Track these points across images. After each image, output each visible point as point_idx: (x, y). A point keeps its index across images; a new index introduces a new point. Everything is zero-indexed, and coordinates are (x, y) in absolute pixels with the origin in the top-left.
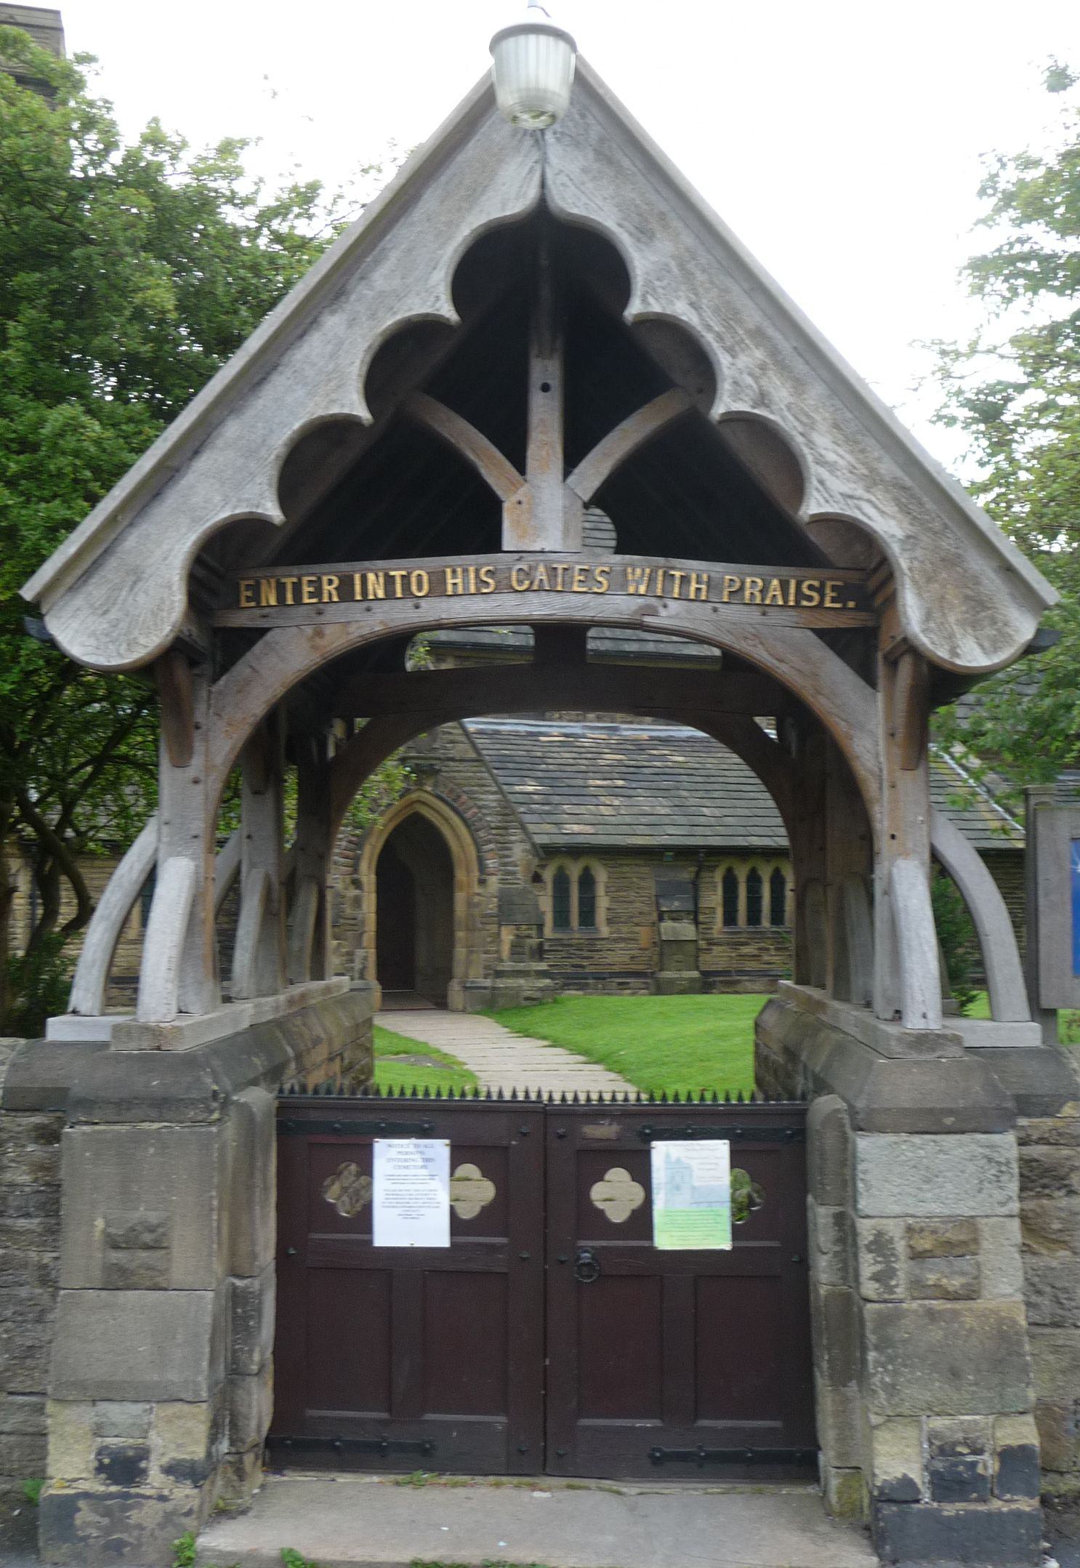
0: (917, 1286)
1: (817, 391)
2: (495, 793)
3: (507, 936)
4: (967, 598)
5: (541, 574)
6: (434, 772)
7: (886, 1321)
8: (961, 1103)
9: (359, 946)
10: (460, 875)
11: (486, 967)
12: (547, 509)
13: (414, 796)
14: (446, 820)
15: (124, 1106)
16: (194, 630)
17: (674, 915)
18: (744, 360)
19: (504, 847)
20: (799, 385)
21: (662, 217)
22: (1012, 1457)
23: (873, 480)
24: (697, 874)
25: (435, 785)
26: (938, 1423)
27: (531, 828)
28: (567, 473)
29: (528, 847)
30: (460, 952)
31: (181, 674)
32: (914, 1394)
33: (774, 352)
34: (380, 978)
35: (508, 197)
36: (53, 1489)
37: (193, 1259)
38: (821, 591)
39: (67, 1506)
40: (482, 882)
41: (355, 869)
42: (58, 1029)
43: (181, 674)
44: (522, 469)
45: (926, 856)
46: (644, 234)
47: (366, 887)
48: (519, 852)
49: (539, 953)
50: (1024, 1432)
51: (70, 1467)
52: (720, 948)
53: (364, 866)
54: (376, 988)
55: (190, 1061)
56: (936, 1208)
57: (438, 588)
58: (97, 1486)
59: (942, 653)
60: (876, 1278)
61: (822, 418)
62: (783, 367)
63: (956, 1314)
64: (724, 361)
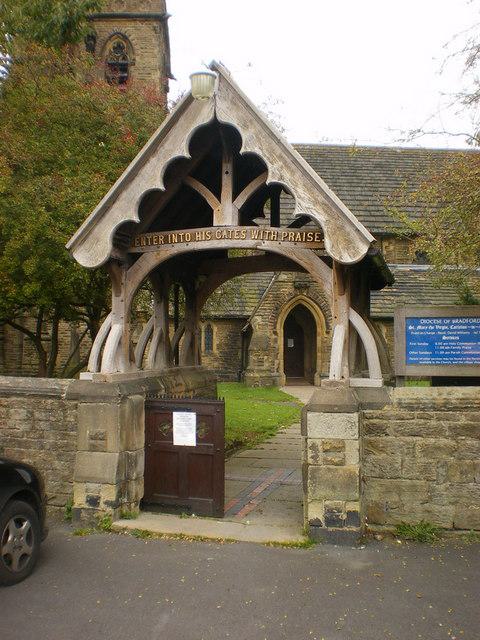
0: (325, 461)
1: (298, 174)
4: (346, 240)
5: (225, 233)
6: (307, 287)
7: (314, 471)
8: (340, 403)
10: (319, 330)
12: (226, 212)
15: (94, 398)
16: (118, 255)
18: (275, 166)
20: (292, 172)
21: (251, 121)
22: (352, 515)
23: (316, 202)
26: (327, 503)
28: (233, 200)
31: (114, 268)
32: (321, 493)
33: (285, 163)
35: (204, 118)
36: (76, 506)
37: (113, 442)
38: (313, 236)
39: (79, 511)
42: (83, 376)
43: (114, 268)
44: (219, 200)
45: (347, 323)
46: (245, 126)
50: (355, 507)
51: (80, 501)
53: (278, 326)
55: (112, 385)
56: (331, 436)
57: (193, 239)
58: (86, 506)
59: (337, 258)
60: (312, 457)
61: (300, 183)
62: (288, 167)
63: (337, 470)
64: (269, 165)
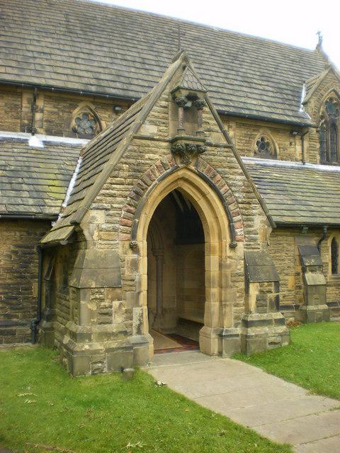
2: (241, 174)
3: (254, 290)
9: (137, 303)
11: (236, 318)
13: (180, 173)
14: (204, 195)
17: (312, 268)
19: (248, 218)
24: (320, 242)
25: (196, 165)
27: (268, 206)
29: (265, 218)
30: (213, 305)
34: (152, 330)
40: (233, 247)
41: (134, 237)
47: (141, 252)
48: (259, 222)
49: (277, 305)
52: (331, 288)
54: (151, 340)
